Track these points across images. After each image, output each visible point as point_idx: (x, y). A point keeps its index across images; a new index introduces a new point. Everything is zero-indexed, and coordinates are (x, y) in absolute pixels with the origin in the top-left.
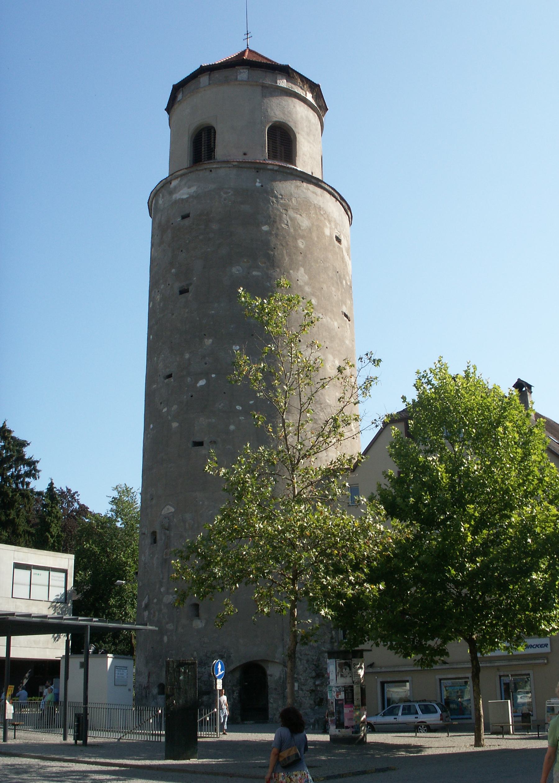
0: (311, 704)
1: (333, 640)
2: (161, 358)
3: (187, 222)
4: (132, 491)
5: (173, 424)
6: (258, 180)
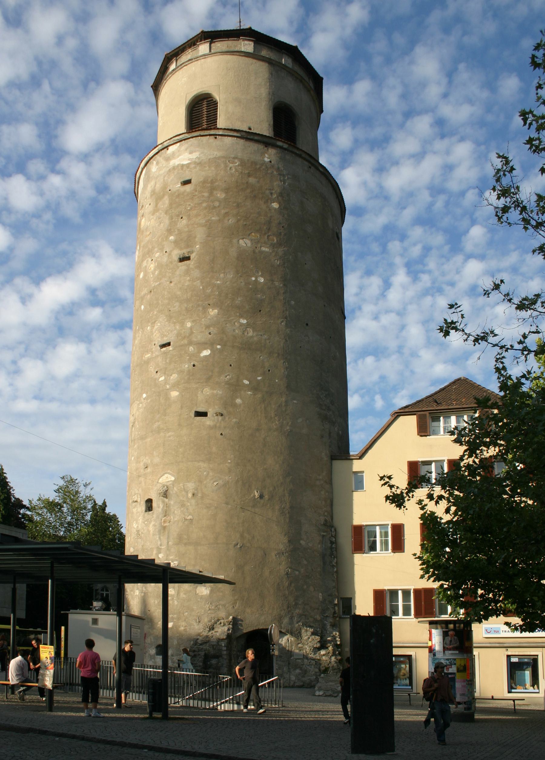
0: (316, 672)
1: (336, 615)
2: (156, 327)
3: (188, 187)
4: (77, 482)
5: (171, 393)
6: (266, 155)
